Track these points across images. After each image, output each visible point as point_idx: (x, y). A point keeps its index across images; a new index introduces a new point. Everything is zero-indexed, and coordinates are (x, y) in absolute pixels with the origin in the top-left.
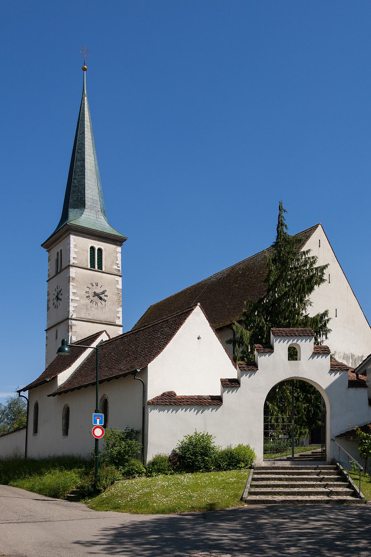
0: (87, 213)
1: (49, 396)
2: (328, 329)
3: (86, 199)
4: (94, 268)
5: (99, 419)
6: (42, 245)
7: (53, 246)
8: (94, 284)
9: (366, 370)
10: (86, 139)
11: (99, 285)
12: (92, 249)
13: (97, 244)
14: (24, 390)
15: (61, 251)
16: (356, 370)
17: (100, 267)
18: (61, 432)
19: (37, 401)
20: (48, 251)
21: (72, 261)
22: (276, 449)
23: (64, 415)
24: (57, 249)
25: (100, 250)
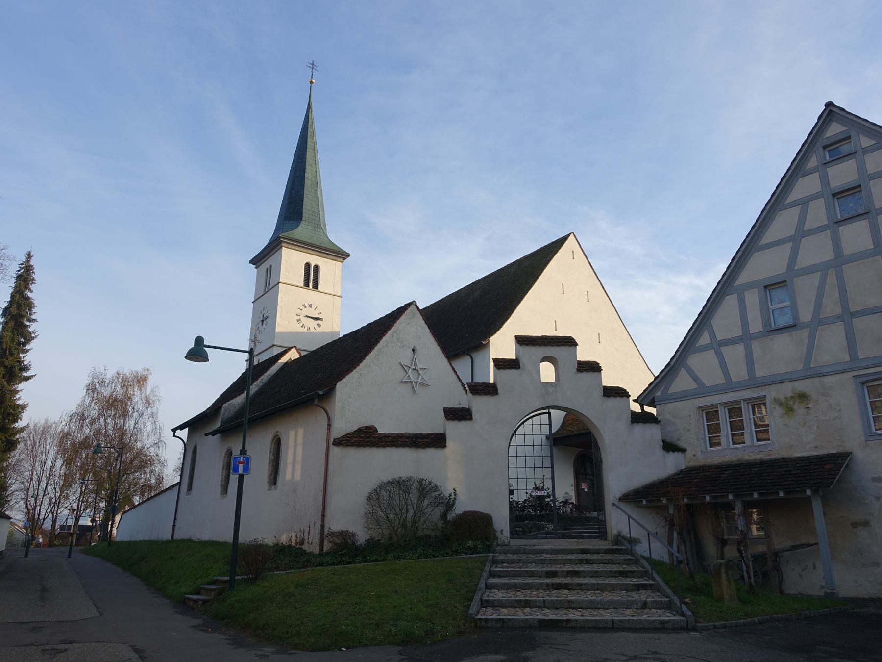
0: (304, 226)
1: (207, 435)
3: (304, 211)
5: (242, 465)
7: (263, 261)
8: (307, 306)
9: (654, 398)
10: (308, 150)
12: (308, 265)
13: (314, 260)
14: (181, 427)
15: (271, 266)
16: (640, 399)
17: (316, 286)
18: (219, 489)
19: (196, 443)
21: (281, 281)
22: (117, 391)
23: (225, 464)
24: (265, 265)
25: (317, 268)
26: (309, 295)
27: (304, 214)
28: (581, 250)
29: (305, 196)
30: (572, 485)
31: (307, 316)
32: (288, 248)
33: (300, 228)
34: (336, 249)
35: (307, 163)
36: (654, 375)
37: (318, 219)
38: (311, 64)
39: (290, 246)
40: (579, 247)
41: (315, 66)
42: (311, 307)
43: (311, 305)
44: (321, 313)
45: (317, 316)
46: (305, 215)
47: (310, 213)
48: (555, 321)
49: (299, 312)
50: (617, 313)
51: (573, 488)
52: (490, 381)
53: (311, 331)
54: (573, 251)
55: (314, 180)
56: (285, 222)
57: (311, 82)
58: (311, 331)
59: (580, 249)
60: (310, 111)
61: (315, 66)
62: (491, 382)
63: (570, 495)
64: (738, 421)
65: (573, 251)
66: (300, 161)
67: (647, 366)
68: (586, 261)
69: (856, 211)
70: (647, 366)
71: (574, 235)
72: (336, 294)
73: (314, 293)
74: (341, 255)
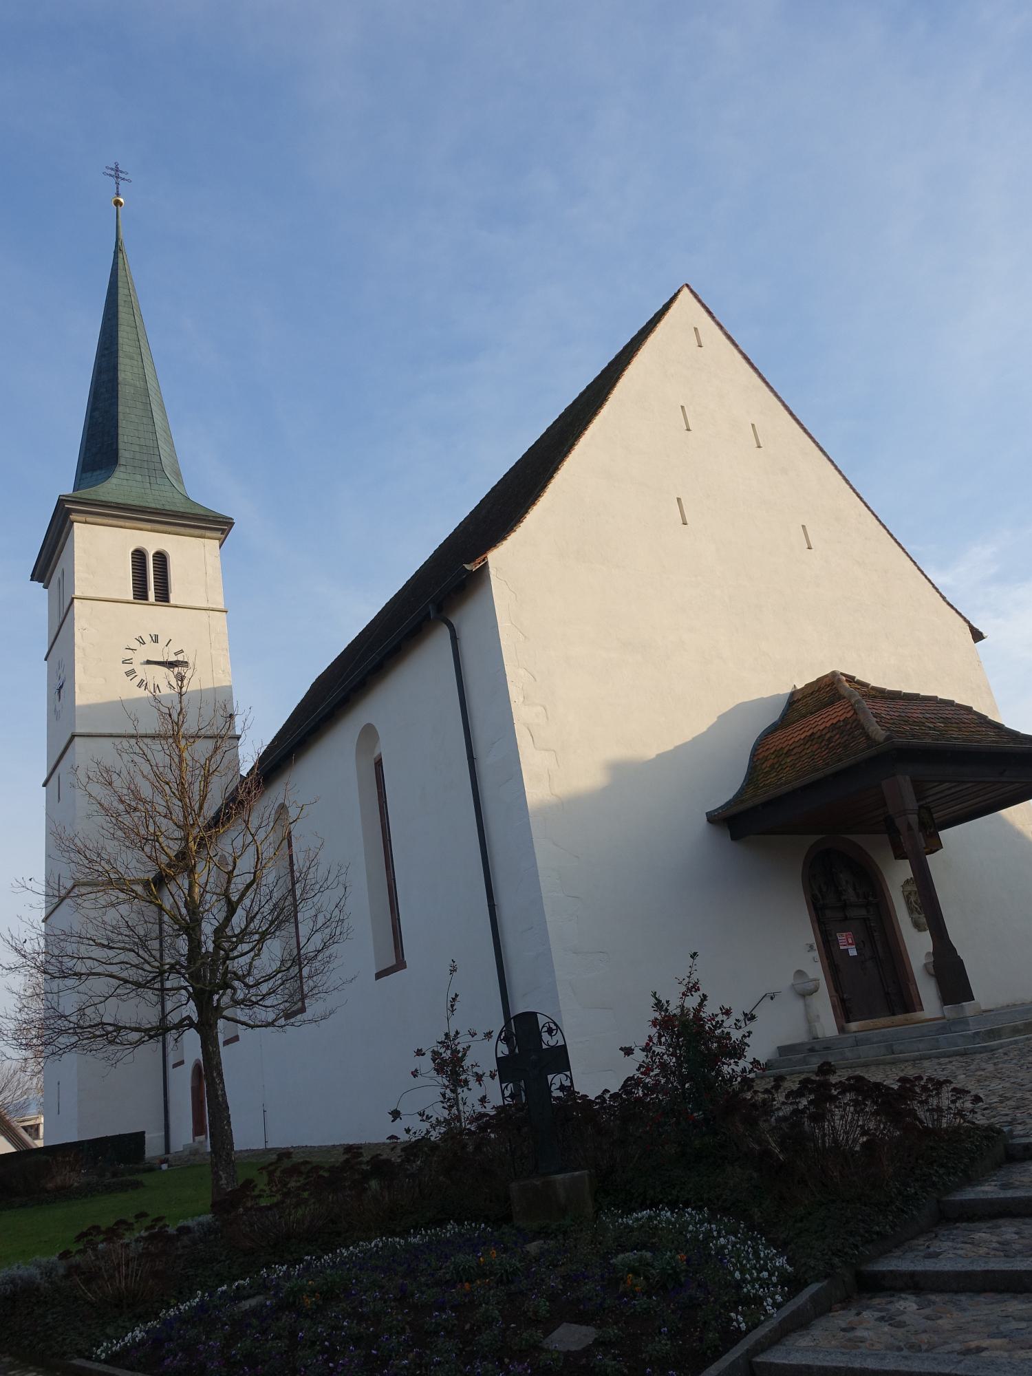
0: (122, 476)
2: (780, 723)
3: (121, 446)
4: (147, 599)
6: (31, 580)
8: (147, 639)
10: (121, 328)
11: (163, 640)
12: (139, 557)
13: (152, 541)
17: (163, 595)
20: (45, 587)
21: (77, 593)
25: (161, 558)
26: (150, 616)
27: (121, 453)
28: (717, 328)
29: (121, 416)
30: (811, 947)
31: (149, 662)
32: (86, 522)
33: (113, 481)
34: (202, 512)
35: (120, 354)
37: (156, 459)
38: (112, 169)
39: (90, 519)
40: (709, 319)
41: (121, 172)
42: (156, 641)
43: (156, 636)
44: (182, 651)
45: (173, 658)
46: (124, 454)
47: (137, 449)
48: (679, 500)
49: (129, 655)
50: (840, 472)
51: (816, 954)
53: (162, 693)
54: (696, 329)
55: (139, 384)
56: (84, 475)
57: (117, 203)
58: (162, 693)
59: (712, 323)
60: (120, 255)
61: (121, 172)
63: (811, 977)
65: (696, 329)
66: (106, 352)
67: (944, 598)
68: (736, 352)
70: (944, 598)
71: (692, 291)
72: (214, 606)
73: (161, 611)
74: (218, 525)
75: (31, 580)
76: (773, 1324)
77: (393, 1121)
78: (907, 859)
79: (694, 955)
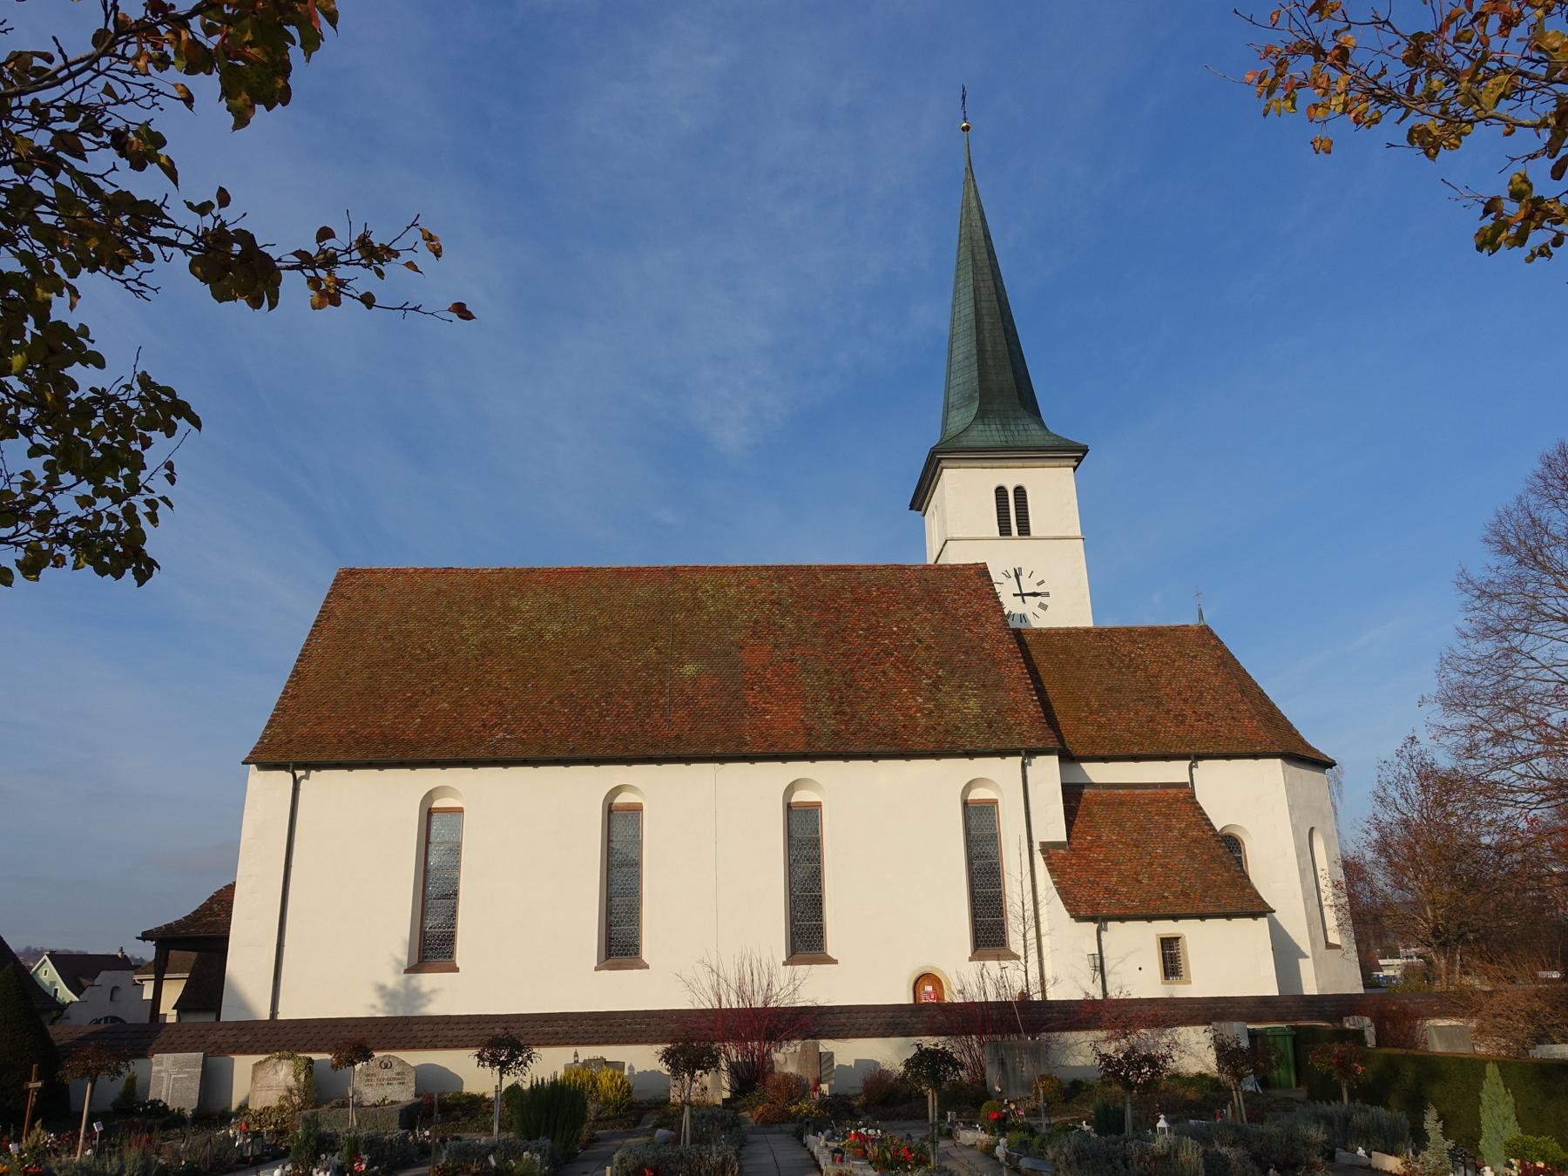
6: (910, 509)
12: (1001, 492)
13: (1010, 477)
17: (1024, 530)
25: (1020, 492)
36: (88, 150)
44: (1043, 582)
52: (1302, 990)
62: (1306, 993)
64: (1248, 1105)
69: (1051, 888)
75: (910, 509)
76: (1499, 85)
77: (138, 938)
78: (151, 1021)
79: (461, 310)
